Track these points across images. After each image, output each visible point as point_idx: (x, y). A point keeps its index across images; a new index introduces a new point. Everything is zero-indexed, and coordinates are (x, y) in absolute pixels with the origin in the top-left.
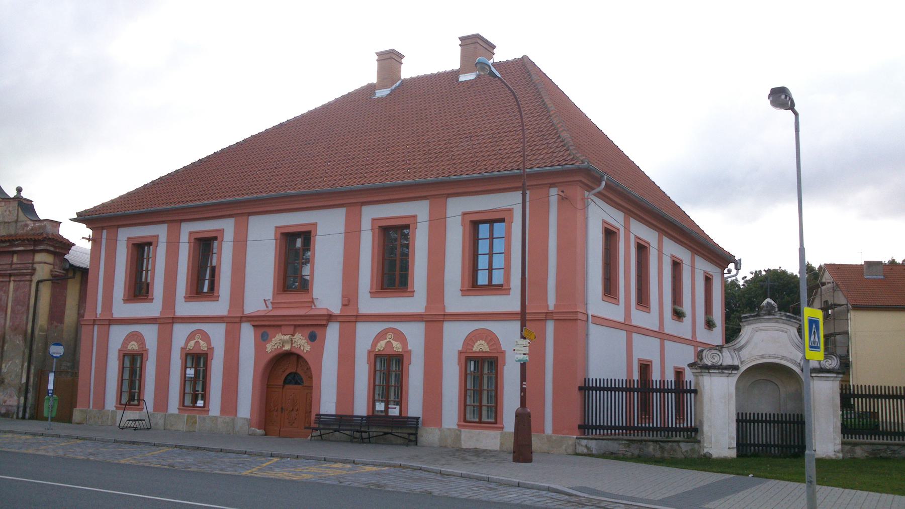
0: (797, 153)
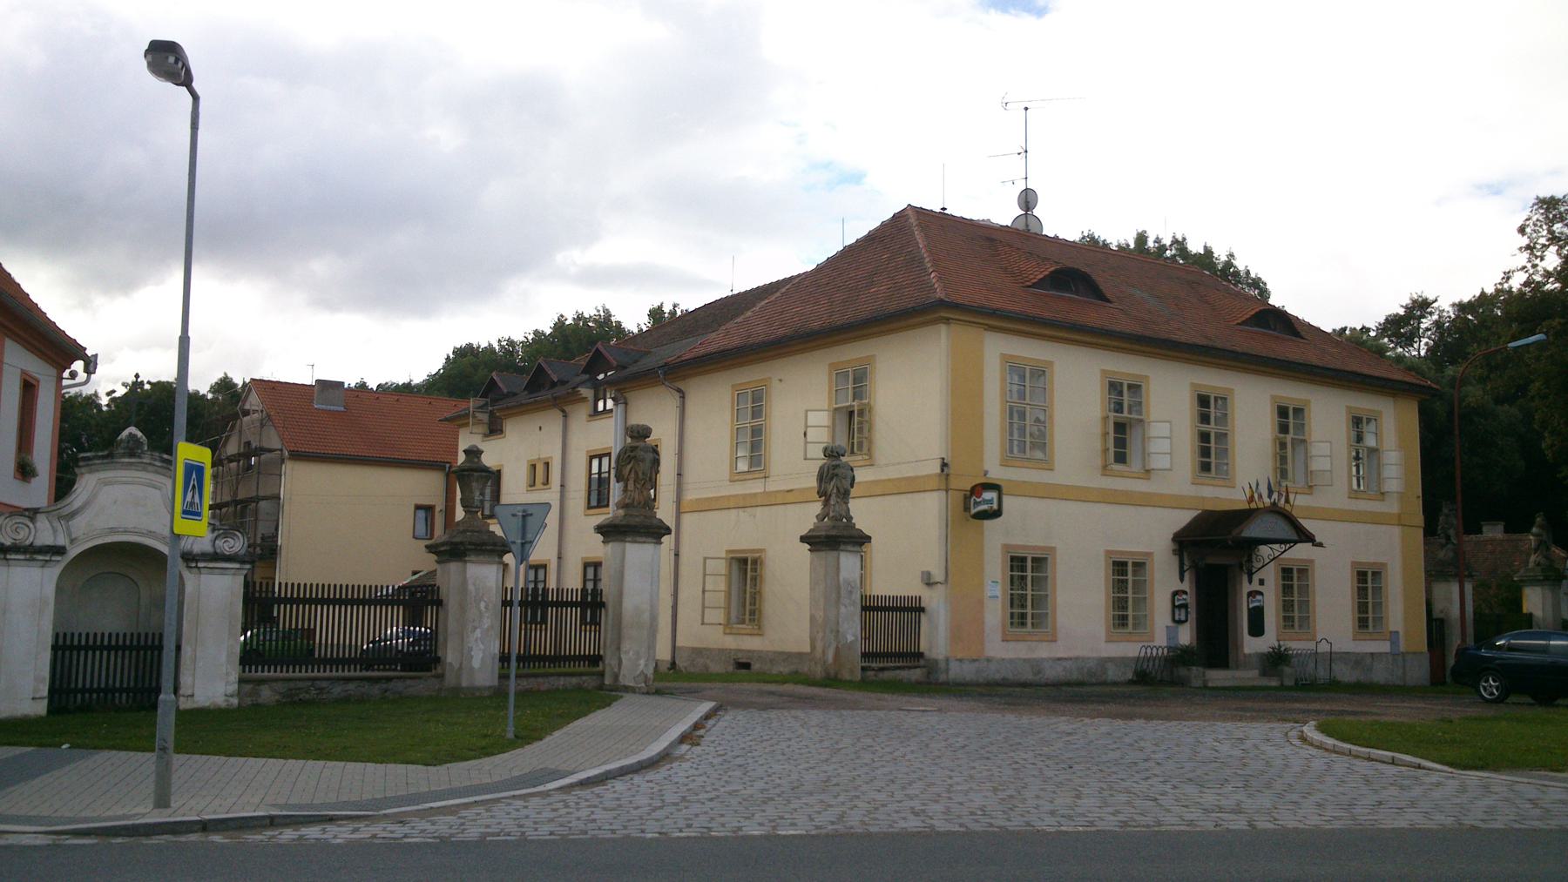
0: (190, 170)
